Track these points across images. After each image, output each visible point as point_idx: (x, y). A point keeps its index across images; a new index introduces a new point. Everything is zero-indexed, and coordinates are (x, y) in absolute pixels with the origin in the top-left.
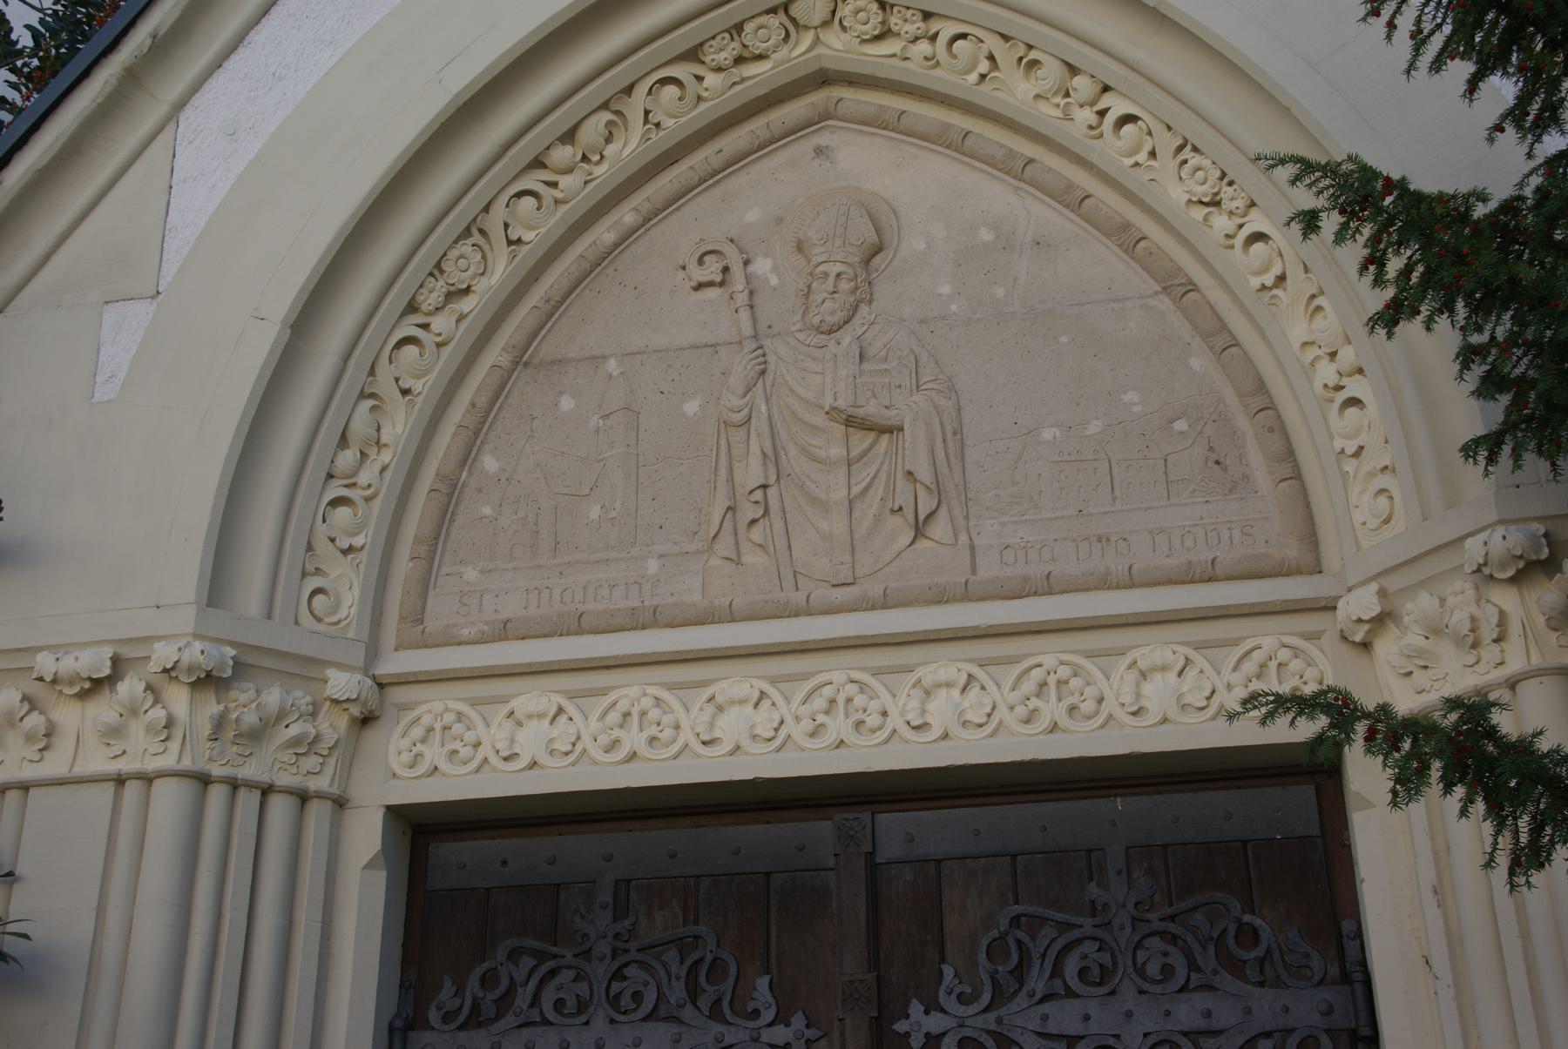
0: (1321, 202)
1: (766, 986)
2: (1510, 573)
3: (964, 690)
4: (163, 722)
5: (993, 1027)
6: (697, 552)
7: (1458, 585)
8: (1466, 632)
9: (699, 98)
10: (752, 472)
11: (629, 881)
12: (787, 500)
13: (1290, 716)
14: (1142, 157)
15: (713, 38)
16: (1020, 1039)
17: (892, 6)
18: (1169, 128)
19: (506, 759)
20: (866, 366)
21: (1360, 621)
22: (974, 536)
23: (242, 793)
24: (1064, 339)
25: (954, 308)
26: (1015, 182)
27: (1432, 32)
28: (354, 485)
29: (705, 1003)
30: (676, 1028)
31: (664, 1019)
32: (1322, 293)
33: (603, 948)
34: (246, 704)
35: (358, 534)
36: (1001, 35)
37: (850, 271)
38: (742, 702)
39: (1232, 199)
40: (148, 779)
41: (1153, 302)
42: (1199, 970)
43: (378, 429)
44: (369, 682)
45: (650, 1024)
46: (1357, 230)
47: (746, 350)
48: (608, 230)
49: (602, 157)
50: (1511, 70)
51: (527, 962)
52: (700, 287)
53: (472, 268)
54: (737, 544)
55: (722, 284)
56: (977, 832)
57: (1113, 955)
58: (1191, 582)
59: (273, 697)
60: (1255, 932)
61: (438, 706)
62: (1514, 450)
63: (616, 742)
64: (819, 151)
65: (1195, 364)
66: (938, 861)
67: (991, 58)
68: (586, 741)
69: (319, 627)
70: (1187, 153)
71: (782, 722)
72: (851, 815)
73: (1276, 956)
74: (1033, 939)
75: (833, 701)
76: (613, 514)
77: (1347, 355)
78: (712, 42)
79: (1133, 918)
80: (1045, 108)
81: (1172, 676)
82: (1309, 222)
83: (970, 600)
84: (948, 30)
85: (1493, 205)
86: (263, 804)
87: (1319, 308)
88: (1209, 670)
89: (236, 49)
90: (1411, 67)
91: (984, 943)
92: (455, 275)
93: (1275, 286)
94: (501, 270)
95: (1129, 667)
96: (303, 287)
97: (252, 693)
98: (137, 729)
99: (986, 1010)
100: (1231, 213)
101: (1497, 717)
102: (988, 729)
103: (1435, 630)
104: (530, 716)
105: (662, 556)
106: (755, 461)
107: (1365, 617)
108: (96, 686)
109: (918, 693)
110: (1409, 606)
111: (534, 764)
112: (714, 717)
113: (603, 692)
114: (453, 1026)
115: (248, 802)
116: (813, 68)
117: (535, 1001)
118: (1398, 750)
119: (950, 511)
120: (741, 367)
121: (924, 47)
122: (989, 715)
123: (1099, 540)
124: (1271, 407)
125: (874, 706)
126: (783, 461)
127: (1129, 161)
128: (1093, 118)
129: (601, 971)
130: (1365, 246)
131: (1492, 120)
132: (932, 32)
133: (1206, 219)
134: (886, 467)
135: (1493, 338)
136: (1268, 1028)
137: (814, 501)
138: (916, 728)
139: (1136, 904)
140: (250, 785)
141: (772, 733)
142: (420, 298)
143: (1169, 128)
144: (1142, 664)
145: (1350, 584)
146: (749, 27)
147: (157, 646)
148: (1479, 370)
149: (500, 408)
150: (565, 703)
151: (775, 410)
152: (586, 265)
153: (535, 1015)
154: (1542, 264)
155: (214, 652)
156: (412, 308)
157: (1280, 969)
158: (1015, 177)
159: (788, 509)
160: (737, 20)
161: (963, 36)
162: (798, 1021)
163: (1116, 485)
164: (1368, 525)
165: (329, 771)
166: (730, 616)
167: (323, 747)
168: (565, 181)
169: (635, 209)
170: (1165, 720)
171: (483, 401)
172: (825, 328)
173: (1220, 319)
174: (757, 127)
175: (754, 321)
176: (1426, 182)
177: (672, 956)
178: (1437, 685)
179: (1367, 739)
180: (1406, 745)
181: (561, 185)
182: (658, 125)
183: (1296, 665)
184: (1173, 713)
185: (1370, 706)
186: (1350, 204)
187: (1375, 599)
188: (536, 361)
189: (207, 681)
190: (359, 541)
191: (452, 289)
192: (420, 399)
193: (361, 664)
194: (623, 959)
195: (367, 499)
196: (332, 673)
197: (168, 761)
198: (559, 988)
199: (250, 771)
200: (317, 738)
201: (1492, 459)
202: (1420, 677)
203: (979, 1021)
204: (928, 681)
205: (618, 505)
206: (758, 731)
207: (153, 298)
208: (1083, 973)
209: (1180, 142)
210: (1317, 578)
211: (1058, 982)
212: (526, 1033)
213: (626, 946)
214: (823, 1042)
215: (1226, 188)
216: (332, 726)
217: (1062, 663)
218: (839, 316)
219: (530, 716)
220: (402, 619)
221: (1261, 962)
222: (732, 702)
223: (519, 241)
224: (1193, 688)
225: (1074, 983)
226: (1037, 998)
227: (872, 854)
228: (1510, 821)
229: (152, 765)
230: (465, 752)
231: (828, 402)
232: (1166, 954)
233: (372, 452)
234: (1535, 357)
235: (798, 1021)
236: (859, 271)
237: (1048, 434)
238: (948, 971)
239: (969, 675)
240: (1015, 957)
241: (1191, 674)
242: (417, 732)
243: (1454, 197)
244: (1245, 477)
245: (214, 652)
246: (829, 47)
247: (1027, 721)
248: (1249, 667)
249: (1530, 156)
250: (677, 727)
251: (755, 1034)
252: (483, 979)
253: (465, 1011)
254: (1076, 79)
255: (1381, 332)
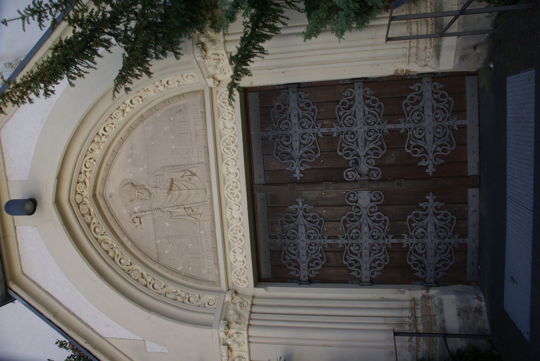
0: (123, 87)
1: (291, 207)
2: (204, 52)
3: (229, 165)
4: (237, 334)
5: (298, 159)
6: (199, 223)
7: (207, 62)
8: (216, 61)
9: (98, 223)
10: (181, 211)
11: (269, 236)
12: (187, 203)
13: (233, 95)
14: (113, 126)
15: (85, 220)
16: (301, 154)
17: (78, 181)
18: (107, 120)
19: (244, 263)
20: (158, 186)
21: (214, 82)
22: (196, 163)
23: (252, 317)
24: (153, 143)
25: (145, 167)
26: (118, 154)
27: (88, 64)
28: (185, 297)
29: (294, 219)
30: (299, 225)
31: (297, 227)
32: (144, 88)
33: (283, 241)
34: (232, 317)
35: (196, 296)
36: (85, 156)
37: (137, 190)
38: (231, 212)
39: (123, 107)
40: (249, 337)
41: (145, 124)
42: (286, 117)
43: (173, 292)
44: (228, 292)
45: (299, 231)
46: (130, 80)
47: (155, 212)
48: (128, 243)
49: (112, 245)
50: (97, 49)
51: (286, 257)
52: (141, 223)
53: (137, 273)
54: (197, 214)
55: (140, 218)
56: (259, 163)
57: (283, 135)
58: (205, 117)
59: (231, 312)
60: (278, 106)
61: (233, 278)
62: (178, 49)
63: (240, 239)
64: (110, 197)
65: (158, 115)
66: (265, 171)
67: (90, 159)
68: (240, 246)
69: (216, 303)
70: (112, 117)
71: (236, 204)
72: (255, 189)
73: (283, 102)
74: (281, 151)
75: (231, 193)
76: (191, 241)
77: (157, 83)
78: (86, 220)
79: (276, 130)
80: (102, 147)
81: (226, 121)
82: (127, 89)
83: (209, 164)
84: (84, 168)
85: (126, 53)
86: (254, 313)
87: (147, 89)
88: (224, 113)
89: (88, 325)
90: (95, 68)
91: (281, 161)
92: (139, 276)
93: (142, 98)
94: (137, 266)
95: (224, 130)
96: (142, 309)
97: (231, 317)
98: (238, 340)
99: (295, 161)
100: (126, 107)
101: (233, 55)
102: (237, 160)
103: (216, 67)
104: (235, 258)
105: (200, 231)
106: (179, 210)
107: (213, 81)
108: (229, 348)
109: (229, 175)
110: (211, 72)
111: (245, 257)
112: (235, 218)
113: (229, 242)
114: (299, 271)
115: (253, 316)
116: (92, 198)
117: (294, 255)
118: (240, 74)
119: (190, 168)
120: (158, 214)
121: (87, 174)
122: (234, 160)
123: (196, 136)
124: (168, 100)
125: (232, 184)
126: (179, 204)
127: (114, 129)
128: (104, 137)
129: (288, 241)
130: (133, 79)
131: (107, 52)
132: (84, 172)
133: (127, 113)
134: (180, 182)
135: (154, 53)
136: (297, 104)
137: (188, 197)
138: (237, 175)
139: (273, 130)
140: (250, 316)
141: (238, 206)
142: (144, 284)
143: (107, 120)
144: (223, 127)
145: (206, 84)
146: (82, 212)
147: (221, 337)
148: (161, 56)
149: (168, 266)
150: (232, 250)
151: (168, 206)
152: (136, 248)
153: (297, 255)
154: (139, 43)
155: (222, 325)
156: (146, 286)
157: (285, 101)
158: (117, 154)
159: (189, 203)
160: (81, 215)
161: (85, 165)
162: (298, 200)
163: (185, 132)
164: (194, 80)
165: (247, 300)
166: (213, 215)
167: (242, 301)
168: (117, 253)
169: (123, 237)
170: (235, 123)
171: (166, 270)
172: (150, 195)
173: (149, 110)
174: (105, 210)
175: (148, 211)
176: (120, 66)
177: (285, 227)
178: (227, 67)
179: (238, 81)
180: (239, 73)
181: (118, 254)
182: (104, 232)
183: (223, 96)
184: (233, 121)
185: (231, 80)
186: (124, 81)
187: (209, 79)
188: (157, 259)
189: (228, 326)
190: (197, 296)
191: (141, 277)
192: (166, 284)
193: (224, 294)
194: (285, 237)
195: (188, 294)
196: (226, 300)
197: (245, 333)
198: (291, 250)
199: (247, 316)
200: (240, 303)
201: (180, 54)
202: (226, 71)
203: (297, 162)
204: (226, 173)
205: (189, 240)
206: (237, 209)
207: (145, 341)
208: (287, 141)
209: (110, 118)
210: (205, 91)
211: (289, 146)
212: (301, 256)
213: (283, 236)
214: (302, 195)
215: (120, 109)
216: (237, 299)
217: (223, 144)
218: (147, 192)
219: (235, 258)
220: (214, 286)
221: (284, 105)
222: (231, 215)
223: (131, 263)
224: (228, 117)
225: (289, 143)
226: (292, 150)
227: (263, 185)
228: (254, 54)
229: (246, 336)
230: (243, 271)
231: (166, 195)
232: (283, 124)
233: (178, 293)
234: (158, 44)
235: (298, 200)
236: (137, 188)
237: (173, 147)
238: (287, 169)
239: (225, 164)
240: (284, 155)
241: (225, 117)
242: (238, 282)
243: (124, 60)
244: (183, 105)
245: (222, 325)
246: (87, 195)
247: (235, 152)
248: (224, 105)
249: (116, 45)
250: (237, 226)
251: (300, 209)
252: (290, 266)
253: (296, 269)
254: (95, 140)
255: (152, 75)
